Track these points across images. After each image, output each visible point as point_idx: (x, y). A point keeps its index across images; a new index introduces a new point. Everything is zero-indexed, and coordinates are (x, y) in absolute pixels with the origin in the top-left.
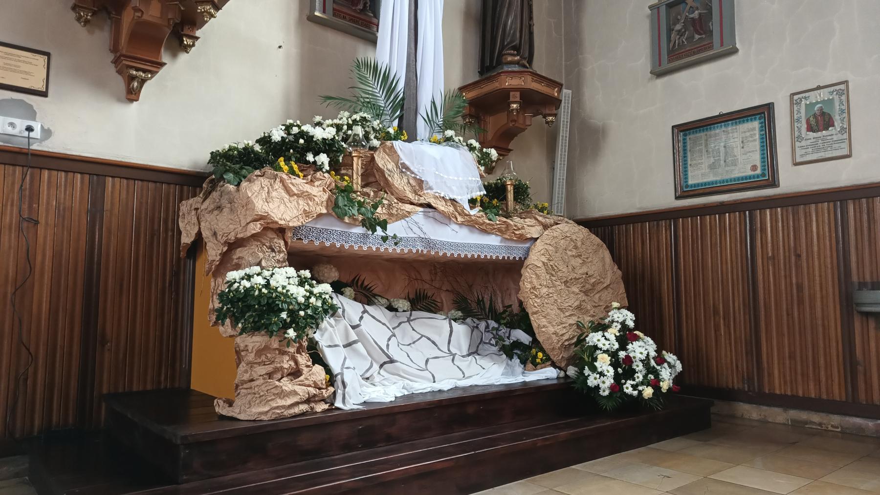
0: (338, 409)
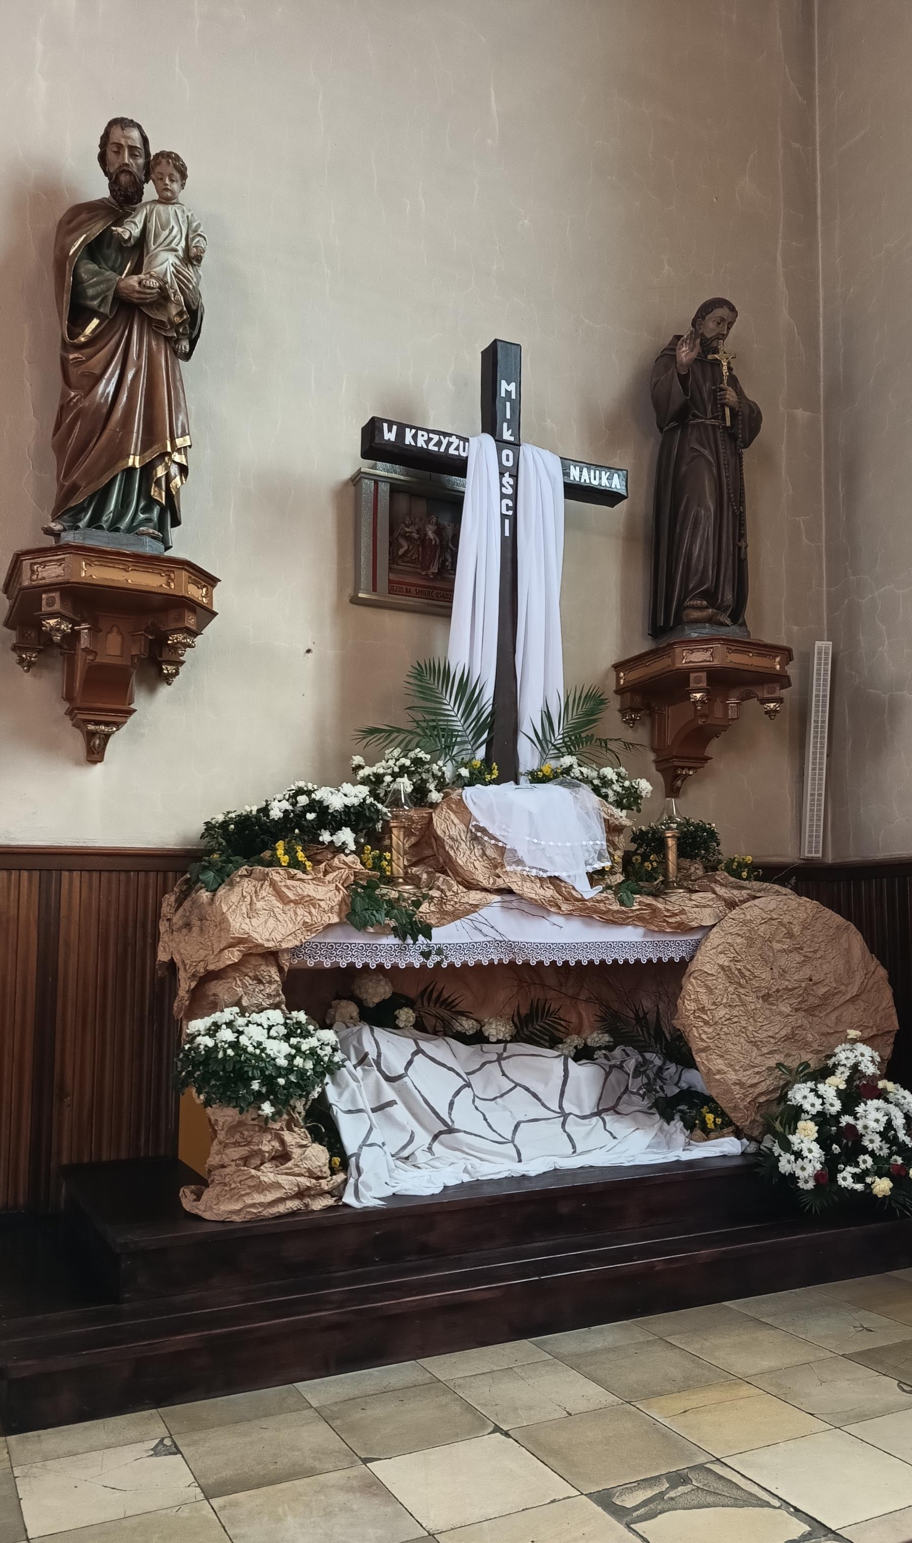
0: (346, 1206)
